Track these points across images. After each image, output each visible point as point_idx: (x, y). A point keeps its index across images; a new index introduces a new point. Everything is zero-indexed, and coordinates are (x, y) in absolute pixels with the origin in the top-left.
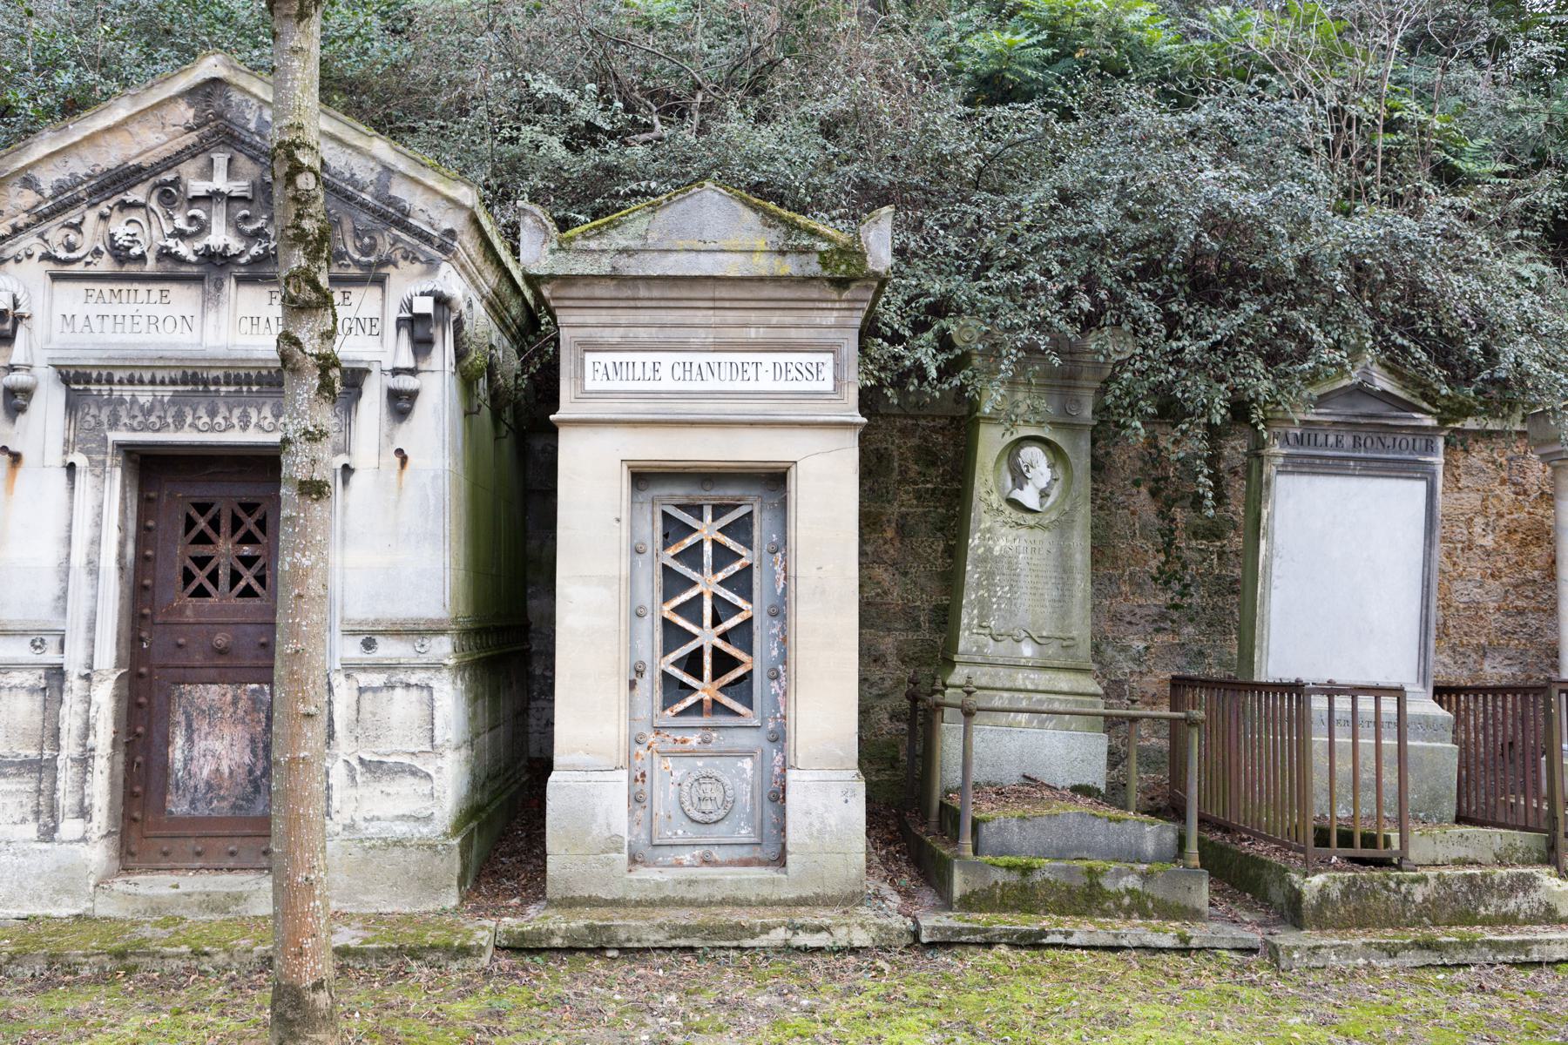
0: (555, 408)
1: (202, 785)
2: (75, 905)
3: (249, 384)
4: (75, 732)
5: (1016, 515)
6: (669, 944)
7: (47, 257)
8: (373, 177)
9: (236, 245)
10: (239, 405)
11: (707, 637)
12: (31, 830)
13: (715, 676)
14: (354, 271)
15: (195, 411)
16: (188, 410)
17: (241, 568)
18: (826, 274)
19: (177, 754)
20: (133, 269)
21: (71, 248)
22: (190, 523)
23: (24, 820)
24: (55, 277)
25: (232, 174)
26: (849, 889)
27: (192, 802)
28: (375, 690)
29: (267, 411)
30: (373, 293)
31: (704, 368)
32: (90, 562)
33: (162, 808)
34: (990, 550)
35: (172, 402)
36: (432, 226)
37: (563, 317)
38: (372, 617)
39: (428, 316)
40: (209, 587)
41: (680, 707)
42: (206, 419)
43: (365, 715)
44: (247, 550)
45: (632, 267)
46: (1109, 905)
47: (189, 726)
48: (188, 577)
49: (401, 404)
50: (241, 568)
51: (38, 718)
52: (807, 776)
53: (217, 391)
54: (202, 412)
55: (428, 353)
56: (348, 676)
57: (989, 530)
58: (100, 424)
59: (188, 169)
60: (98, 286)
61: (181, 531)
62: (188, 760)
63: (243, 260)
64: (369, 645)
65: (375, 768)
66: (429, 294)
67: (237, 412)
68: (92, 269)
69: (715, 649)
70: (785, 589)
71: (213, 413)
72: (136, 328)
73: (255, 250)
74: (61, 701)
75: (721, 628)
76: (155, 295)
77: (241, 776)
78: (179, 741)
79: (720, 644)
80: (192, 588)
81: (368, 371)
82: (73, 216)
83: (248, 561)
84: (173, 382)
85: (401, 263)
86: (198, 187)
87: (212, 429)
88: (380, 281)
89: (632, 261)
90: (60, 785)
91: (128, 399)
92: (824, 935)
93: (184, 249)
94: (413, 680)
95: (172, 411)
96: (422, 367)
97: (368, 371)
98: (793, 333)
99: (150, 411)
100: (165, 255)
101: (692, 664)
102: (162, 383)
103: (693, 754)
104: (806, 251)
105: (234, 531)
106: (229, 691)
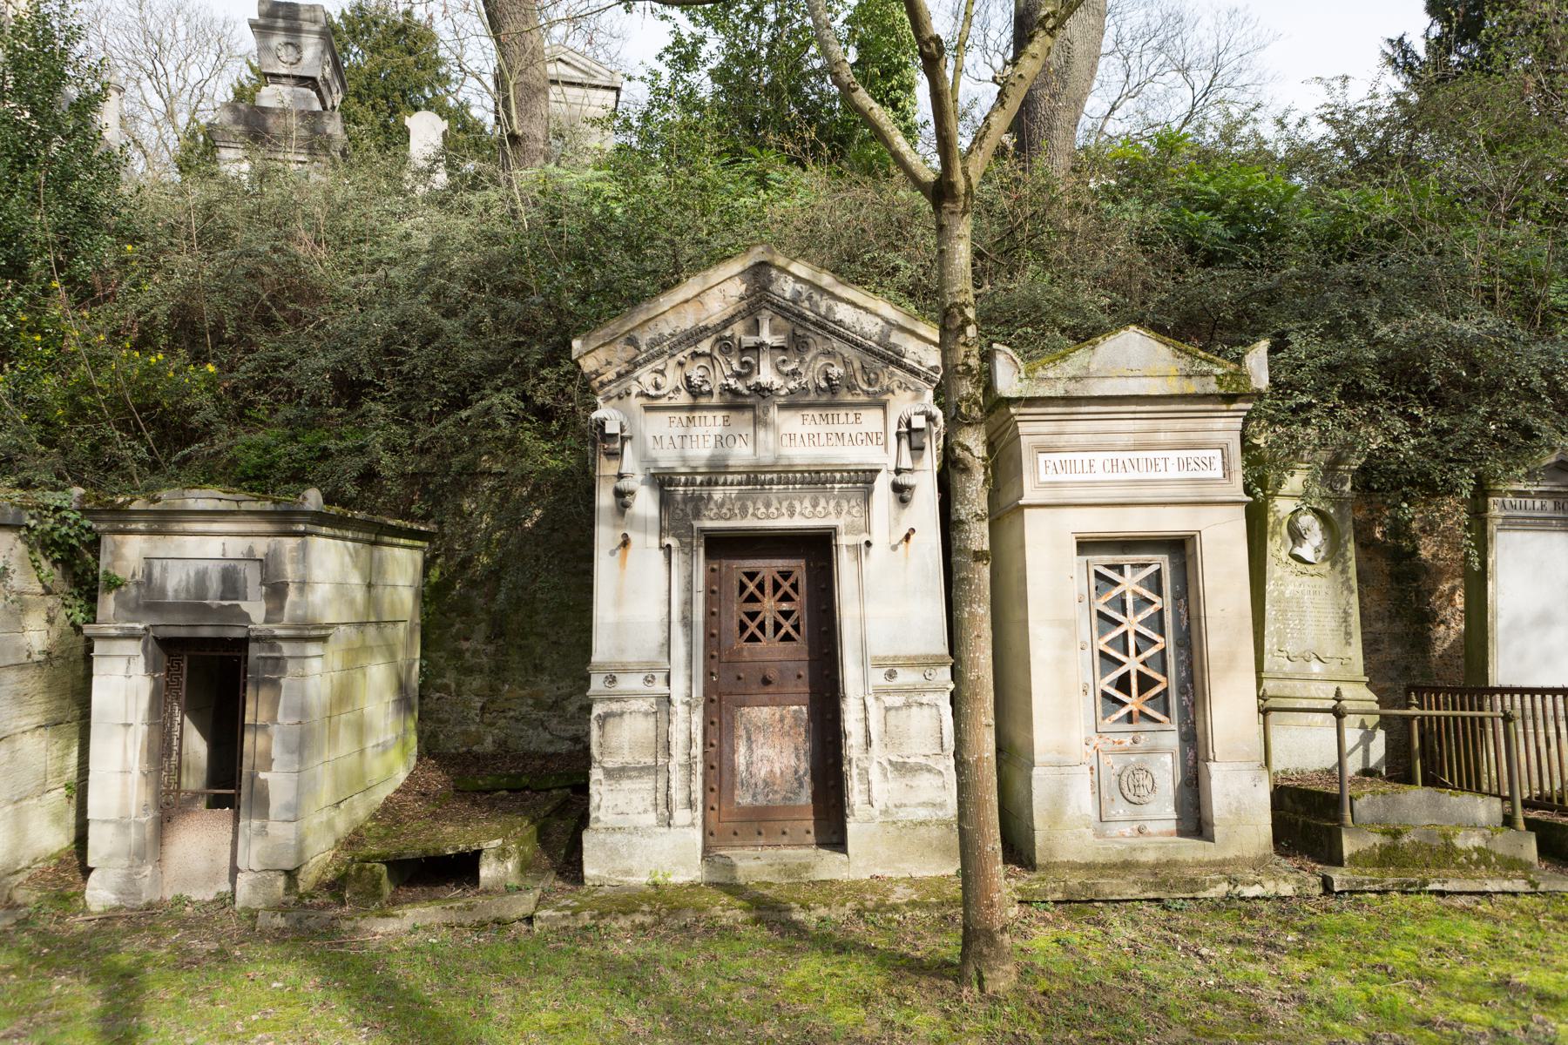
0: (1021, 497)
1: (761, 784)
2: (688, 874)
4: (680, 745)
5: (1301, 566)
6: (1142, 896)
7: (642, 394)
8: (877, 329)
9: (778, 382)
11: (1133, 664)
12: (651, 819)
13: (1140, 693)
14: (863, 398)
16: (750, 504)
17: (781, 620)
18: (1222, 391)
19: (741, 759)
20: (703, 401)
21: (657, 387)
22: (743, 587)
23: (645, 811)
24: (648, 409)
25: (774, 331)
26: (1261, 853)
27: (754, 796)
28: (897, 709)
29: (807, 503)
30: (879, 413)
31: (1127, 464)
32: (684, 618)
33: (732, 800)
34: (1283, 593)
35: (738, 498)
36: (920, 363)
37: (1023, 428)
38: (892, 654)
39: (922, 430)
40: (759, 634)
41: (1116, 717)
42: (763, 510)
43: (891, 728)
44: (785, 606)
45: (1077, 390)
46: (1462, 859)
47: (749, 738)
48: (743, 627)
49: (902, 493)
50: (781, 620)
51: (652, 734)
52: (1224, 767)
55: (921, 457)
56: (877, 699)
57: (1281, 578)
58: (686, 515)
59: (738, 329)
60: (677, 414)
61: (736, 593)
62: (749, 764)
63: (782, 393)
64: (891, 675)
65: (902, 768)
66: (922, 413)
67: (785, 504)
68: (673, 402)
69: (1139, 673)
70: (1189, 626)
71: (768, 505)
73: (792, 385)
74: (669, 721)
75: (1142, 657)
76: (852, 418)
77: (789, 775)
78: (742, 749)
79: (1142, 668)
80: (746, 635)
81: (878, 471)
82: (658, 364)
83: (787, 615)
84: (740, 484)
85: (897, 391)
86: (749, 341)
87: (768, 517)
88: (883, 406)
89: (1078, 385)
90: (673, 784)
92: (1257, 887)
93: (740, 386)
94: (925, 700)
95: (738, 505)
96: (917, 467)
97: (878, 471)
98: (1192, 436)
99: (722, 505)
100: (726, 389)
101: (1123, 684)
103: (1128, 752)
104: (1207, 374)
105: (775, 592)
106: (777, 711)
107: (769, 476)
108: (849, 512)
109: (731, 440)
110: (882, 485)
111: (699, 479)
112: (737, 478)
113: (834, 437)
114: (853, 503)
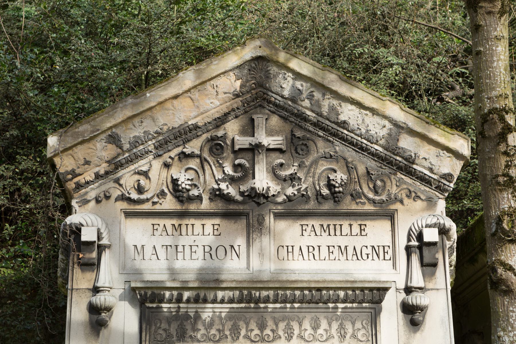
3: (293, 302)
10: (283, 320)
15: (247, 324)
16: (242, 324)
29: (306, 324)
35: (229, 317)
42: (257, 331)
53: (266, 308)
54: (253, 325)
58: (169, 336)
71: (262, 327)
72: (194, 256)
84: (231, 301)
91: (192, 315)
95: (229, 325)
102: (222, 301)
107: (264, 293)
108: (354, 336)
109: (221, 251)
110: (391, 303)
111: (186, 295)
112: (229, 294)
113: (336, 251)
114: (358, 325)
